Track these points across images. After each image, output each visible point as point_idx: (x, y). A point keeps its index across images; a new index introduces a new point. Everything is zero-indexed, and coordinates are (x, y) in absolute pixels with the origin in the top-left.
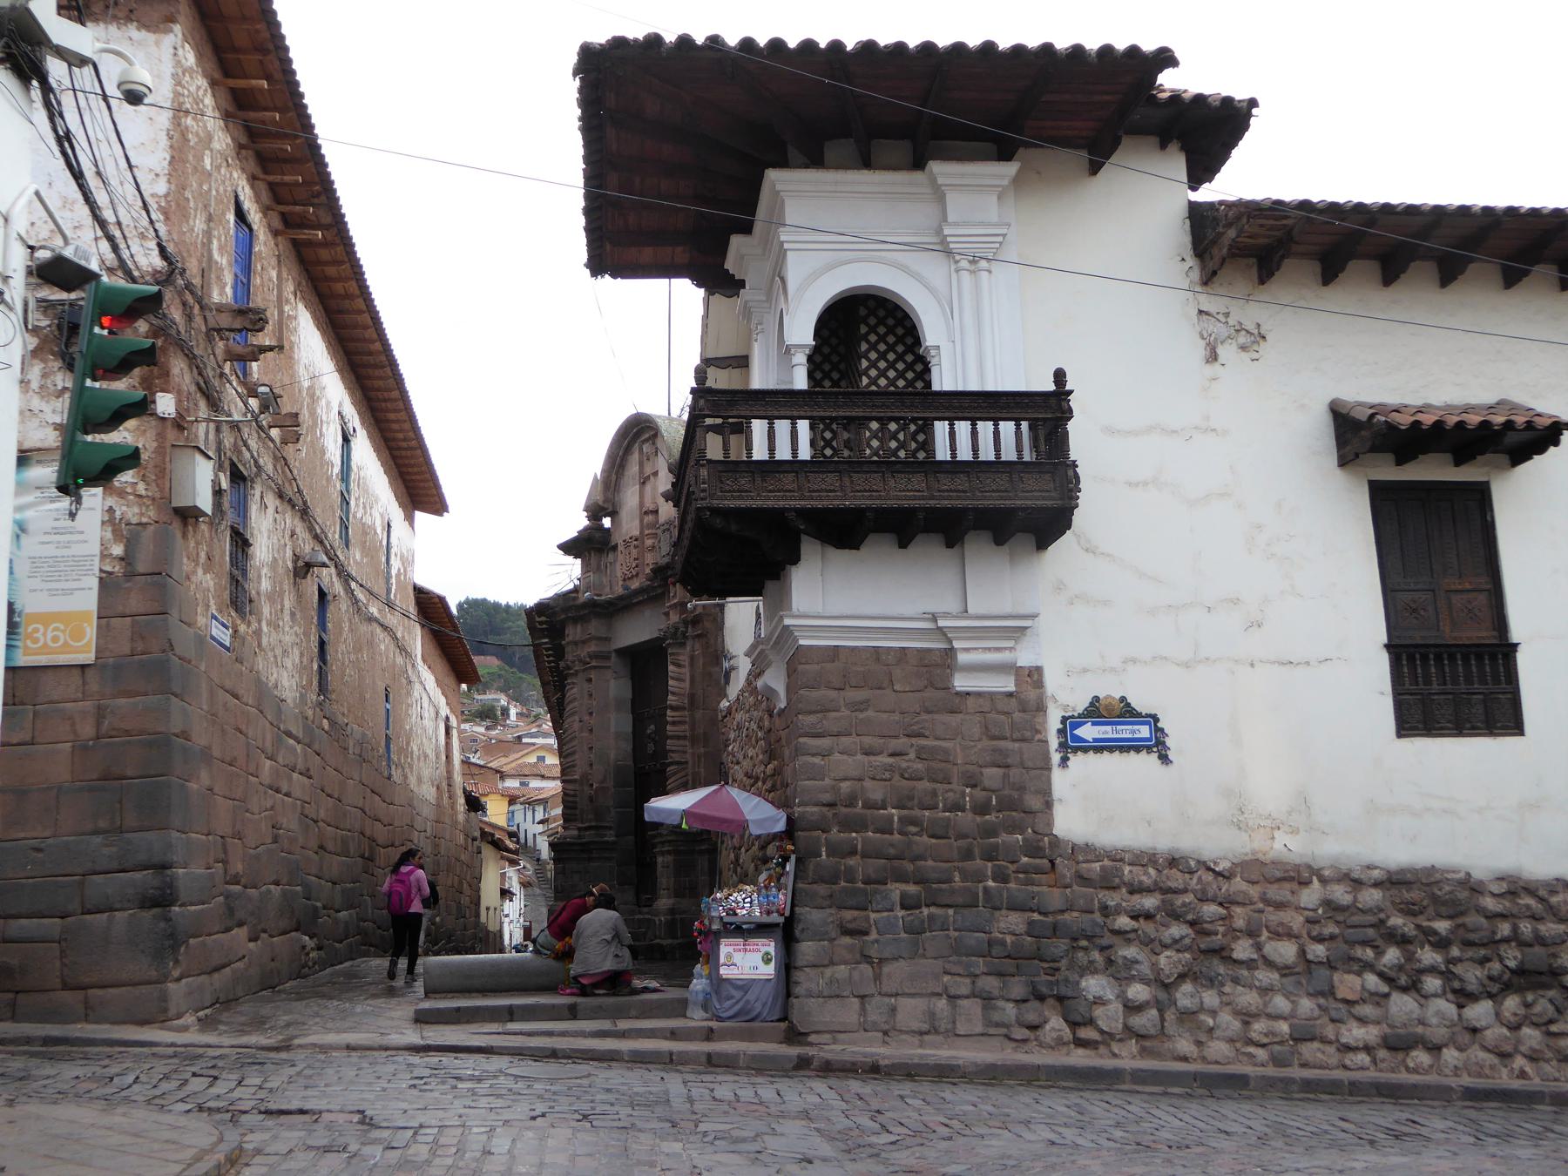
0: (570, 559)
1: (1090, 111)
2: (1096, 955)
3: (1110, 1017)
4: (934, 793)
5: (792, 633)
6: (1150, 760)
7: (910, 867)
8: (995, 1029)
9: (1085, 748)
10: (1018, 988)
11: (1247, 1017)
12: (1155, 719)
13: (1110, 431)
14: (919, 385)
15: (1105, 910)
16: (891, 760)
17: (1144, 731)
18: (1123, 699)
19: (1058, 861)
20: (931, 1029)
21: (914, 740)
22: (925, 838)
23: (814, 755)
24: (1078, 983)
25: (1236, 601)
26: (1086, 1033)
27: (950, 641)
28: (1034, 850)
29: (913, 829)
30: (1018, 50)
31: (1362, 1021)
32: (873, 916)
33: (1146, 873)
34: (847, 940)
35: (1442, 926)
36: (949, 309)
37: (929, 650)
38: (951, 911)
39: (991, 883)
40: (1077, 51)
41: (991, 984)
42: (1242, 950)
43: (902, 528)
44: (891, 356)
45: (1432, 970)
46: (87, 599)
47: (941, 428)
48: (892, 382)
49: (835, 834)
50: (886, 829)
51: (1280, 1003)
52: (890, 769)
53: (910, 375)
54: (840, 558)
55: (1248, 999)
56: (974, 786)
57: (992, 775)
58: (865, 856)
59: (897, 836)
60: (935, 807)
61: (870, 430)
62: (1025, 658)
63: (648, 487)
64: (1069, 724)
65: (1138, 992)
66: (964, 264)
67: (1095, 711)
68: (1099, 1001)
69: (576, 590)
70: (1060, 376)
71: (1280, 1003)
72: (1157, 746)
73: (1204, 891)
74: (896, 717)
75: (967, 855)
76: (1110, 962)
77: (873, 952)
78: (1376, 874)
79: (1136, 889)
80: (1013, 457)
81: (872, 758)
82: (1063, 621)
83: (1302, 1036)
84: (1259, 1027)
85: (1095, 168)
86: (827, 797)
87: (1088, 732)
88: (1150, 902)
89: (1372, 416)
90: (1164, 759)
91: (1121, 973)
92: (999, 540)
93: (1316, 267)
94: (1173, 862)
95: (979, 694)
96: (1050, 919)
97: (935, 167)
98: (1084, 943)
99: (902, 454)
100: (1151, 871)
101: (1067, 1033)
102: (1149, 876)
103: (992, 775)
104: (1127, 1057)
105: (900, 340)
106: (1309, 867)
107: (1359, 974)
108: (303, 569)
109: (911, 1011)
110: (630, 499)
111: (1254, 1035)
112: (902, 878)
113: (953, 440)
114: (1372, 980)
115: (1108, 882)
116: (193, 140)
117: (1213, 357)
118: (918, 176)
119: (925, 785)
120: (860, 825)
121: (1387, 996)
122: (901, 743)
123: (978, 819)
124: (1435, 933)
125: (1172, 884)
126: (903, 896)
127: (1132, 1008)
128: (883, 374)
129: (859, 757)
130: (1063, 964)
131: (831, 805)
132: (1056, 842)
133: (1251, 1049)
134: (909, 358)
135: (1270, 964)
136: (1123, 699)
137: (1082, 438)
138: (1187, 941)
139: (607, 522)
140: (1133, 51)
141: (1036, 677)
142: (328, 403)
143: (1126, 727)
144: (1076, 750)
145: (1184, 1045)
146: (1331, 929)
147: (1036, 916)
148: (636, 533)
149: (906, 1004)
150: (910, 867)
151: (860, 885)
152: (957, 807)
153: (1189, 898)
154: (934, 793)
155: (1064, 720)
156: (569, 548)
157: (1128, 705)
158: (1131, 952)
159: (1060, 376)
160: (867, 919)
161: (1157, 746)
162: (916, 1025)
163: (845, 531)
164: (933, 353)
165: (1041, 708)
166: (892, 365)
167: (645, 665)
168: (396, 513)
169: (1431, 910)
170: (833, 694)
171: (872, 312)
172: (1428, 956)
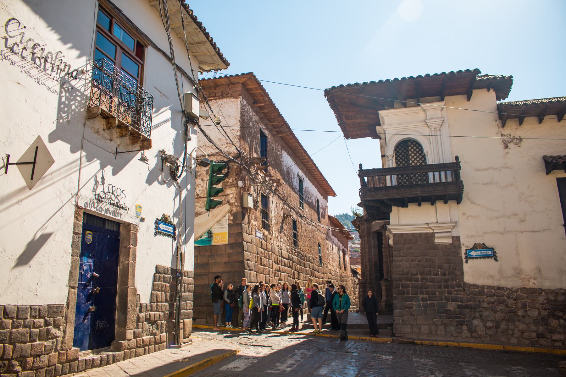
0: (360, 208)
4: (430, 271)
12: (493, 249)
13: (477, 170)
14: (423, 164)
16: (275, 229)
17: (490, 253)
18: (483, 244)
25: (516, 215)
26: (474, 335)
28: (459, 286)
39: (446, 295)
43: (419, 201)
44: (418, 155)
46: (226, 230)
47: (430, 175)
50: (417, 280)
52: (418, 265)
53: (421, 161)
54: (402, 210)
57: (446, 266)
60: (430, 274)
62: (455, 234)
65: (489, 324)
70: (457, 158)
72: (494, 256)
76: (481, 316)
78: (563, 291)
80: (438, 181)
86: (401, 273)
87: (473, 253)
90: (496, 260)
93: (537, 119)
94: (499, 288)
97: (423, 105)
99: (414, 183)
101: (469, 335)
106: (541, 289)
107: (558, 319)
108: (286, 216)
111: (525, 336)
112: (422, 293)
113: (432, 177)
116: (246, 121)
117: (506, 147)
118: (419, 108)
119: (428, 269)
120: (411, 280)
126: (422, 298)
127: (487, 328)
132: (465, 284)
137: (465, 174)
138: (504, 310)
142: (294, 174)
144: (470, 258)
147: (460, 303)
154: (430, 271)
155: (466, 250)
159: (457, 158)
160: (413, 304)
161: (494, 256)
165: (460, 247)
166: (418, 157)
168: (321, 198)
171: (412, 143)
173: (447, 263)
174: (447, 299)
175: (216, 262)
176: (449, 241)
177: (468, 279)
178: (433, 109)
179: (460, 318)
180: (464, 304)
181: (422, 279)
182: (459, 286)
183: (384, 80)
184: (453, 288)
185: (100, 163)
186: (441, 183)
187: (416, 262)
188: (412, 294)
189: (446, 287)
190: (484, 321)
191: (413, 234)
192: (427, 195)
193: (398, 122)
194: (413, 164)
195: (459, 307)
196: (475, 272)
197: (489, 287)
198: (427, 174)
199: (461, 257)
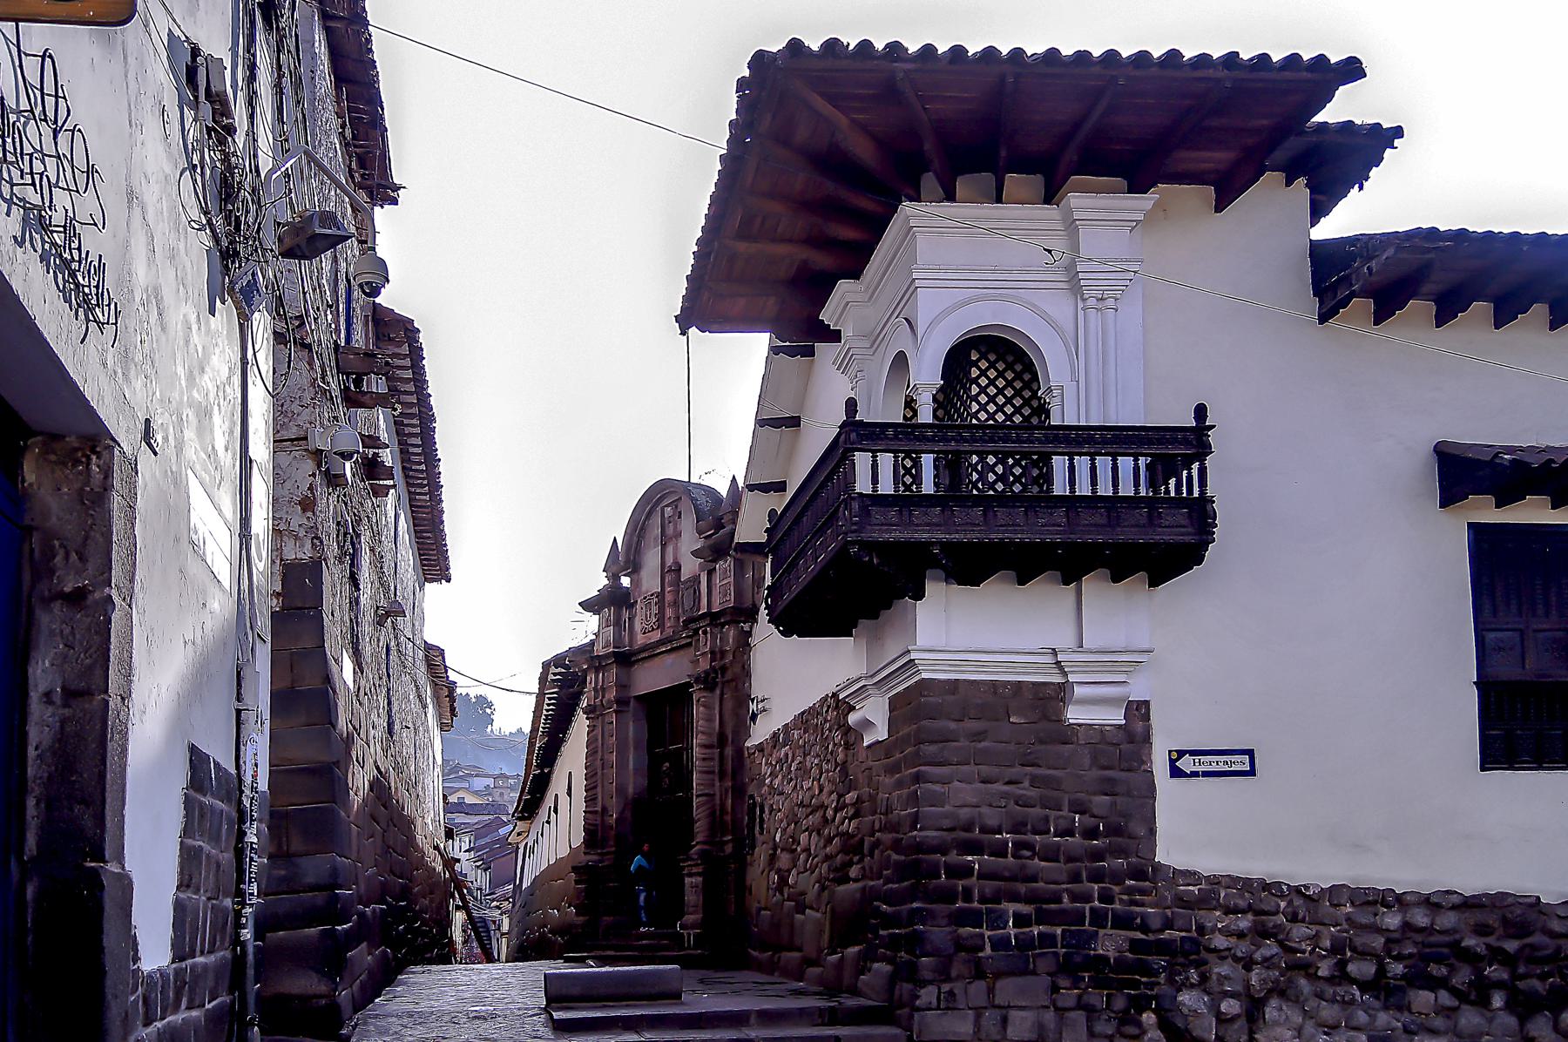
1: (1256, 127)
16: (1006, 788)
27: (1065, 674)
29: (1028, 853)
35: (1511, 946)
43: (1025, 564)
45: (1499, 985)
47: (1059, 463)
48: (1009, 417)
49: (953, 857)
50: (1000, 851)
52: (1004, 796)
57: (1100, 802)
58: (981, 876)
65: (1230, 1006)
66: (1092, 302)
69: (592, 643)
70: (1201, 411)
74: (1012, 747)
75: (1075, 878)
76: (1204, 978)
78: (1455, 899)
86: (946, 823)
88: (1244, 922)
89: (1496, 455)
94: (1265, 886)
103: (1100, 802)
105: (1018, 376)
110: (652, 560)
112: (1014, 897)
113: (1070, 476)
114: (1445, 998)
115: (1205, 901)
118: (1050, 211)
120: (975, 848)
121: (1455, 1009)
122: (1017, 771)
123: (1087, 842)
124: (1504, 950)
125: (1266, 908)
128: (1000, 409)
132: (1158, 867)
134: (1027, 394)
137: (1225, 478)
139: (625, 581)
140: (1321, 60)
151: (976, 904)
154: (1047, 819)
156: (587, 605)
158: (1223, 969)
159: (1201, 411)
160: (982, 936)
163: (970, 567)
165: (1147, 739)
167: (665, 711)
169: (1500, 931)
170: (953, 725)
172: (1493, 971)
174: (1098, 918)
176: (1117, 717)
177: (1168, 853)
178: (1103, 217)
179: (1135, 985)
180: (1151, 937)
181: (1018, 846)
182: (1139, 874)
183: (1096, 53)
184: (1120, 882)
185: (136, 959)
186: (1094, 501)
188: (983, 900)
189: (1096, 877)
190: (1217, 997)
194: (983, 416)
196: (1192, 833)
197: (1233, 881)
198: (1046, 459)
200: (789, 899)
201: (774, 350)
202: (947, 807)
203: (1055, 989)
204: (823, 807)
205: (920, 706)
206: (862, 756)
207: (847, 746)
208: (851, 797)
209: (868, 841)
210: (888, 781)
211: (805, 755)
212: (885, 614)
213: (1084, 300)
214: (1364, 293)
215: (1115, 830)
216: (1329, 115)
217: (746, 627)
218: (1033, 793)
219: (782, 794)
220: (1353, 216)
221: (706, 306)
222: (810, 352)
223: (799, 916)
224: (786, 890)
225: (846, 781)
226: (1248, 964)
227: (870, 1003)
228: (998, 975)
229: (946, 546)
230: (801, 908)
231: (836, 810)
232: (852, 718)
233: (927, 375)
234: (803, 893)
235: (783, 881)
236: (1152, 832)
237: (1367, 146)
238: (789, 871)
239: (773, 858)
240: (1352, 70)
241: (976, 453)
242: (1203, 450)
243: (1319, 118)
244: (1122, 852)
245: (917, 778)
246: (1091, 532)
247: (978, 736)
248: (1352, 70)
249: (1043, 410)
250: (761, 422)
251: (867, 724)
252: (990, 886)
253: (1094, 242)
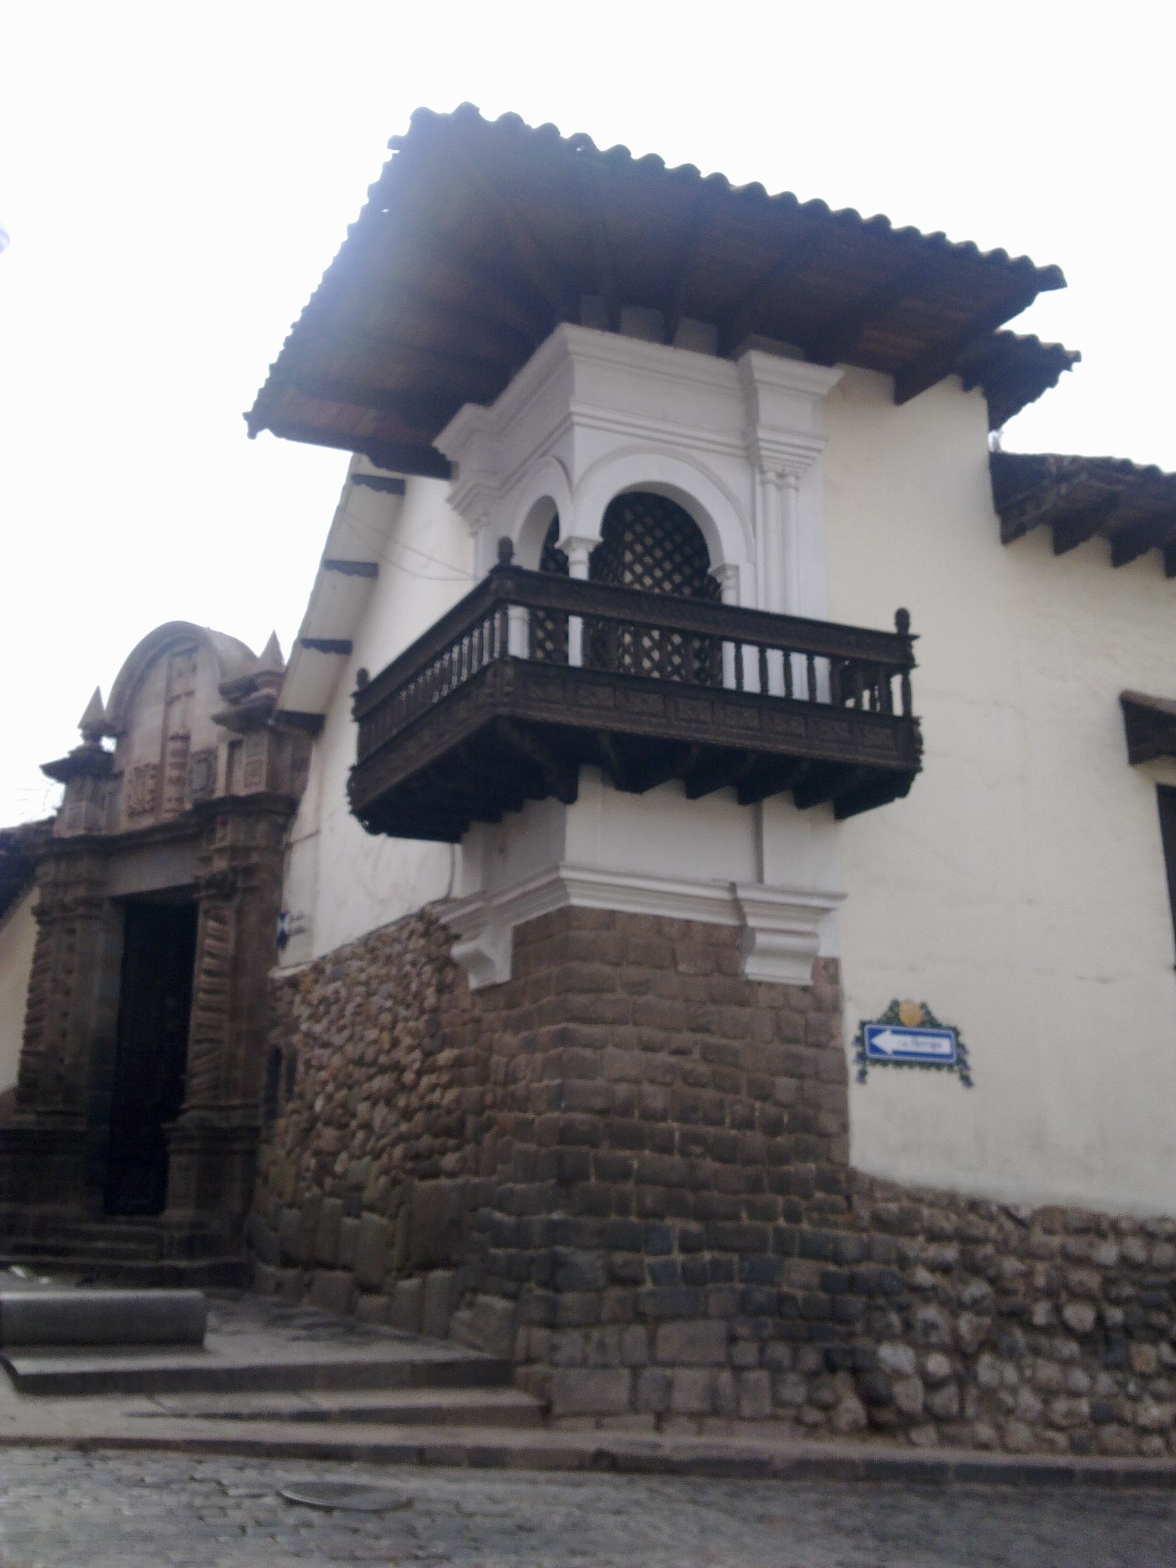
2: (894, 1318)
3: (909, 1395)
4: (720, 1105)
5: (564, 887)
6: (950, 1080)
7: (690, 1197)
8: (780, 1413)
9: (883, 1061)
10: (811, 1359)
11: (1047, 1394)
15: (904, 1262)
16: (673, 1059)
17: (945, 1046)
19: (855, 1198)
20: (715, 1410)
21: (700, 1037)
22: (709, 1161)
23: (585, 1046)
24: (875, 1352)
27: (742, 916)
30: (910, 233)
31: (1158, 1398)
32: (648, 1260)
33: (947, 1218)
34: (617, 1292)
36: (750, 521)
37: (716, 927)
38: (736, 1258)
40: (969, 248)
41: (780, 1351)
42: (1041, 1313)
49: (605, 1151)
51: (1080, 1379)
55: (1048, 1372)
56: (765, 1098)
57: (785, 1086)
59: (677, 1158)
61: (672, 644)
62: (825, 951)
63: (177, 709)
64: (869, 1031)
65: (938, 1364)
66: (771, 476)
67: (893, 1018)
68: (898, 1375)
69: (51, 821)
70: (902, 617)
71: (1080, 1379)
72: (957, 1063)
73: (1006, 1242)
75: (755, 1186)
76: (908, 1325)
77: (649, 1308)
79: (935, 1236)
81: (650, 1055)
82: (864, 908)
83: (1102, 1416)
84: (1061, 1406)
85: (902, 394)
86: (599, 1102)
87: (888, 1042)
88: (950, 1253)
90: (966, 1081)
91: (917, 1338)
92: (803, 801)
94: (974, 1205)
95: (771, 986)
96: (845, 1271)
98: (881, 1301)
100: (953, 1217)
102: (948, 1222)
104: (925, 1448)
109: (689, 1387)
112: (682, 1212)
115: (901, 1225)
120: (634, 1140)
122: (684, 1038)
127: (932, 1384)
129: (637, 1052)
130: (859, 1326)
131: (603, 1112)
132: (853, 1176)
133: (1051, 1434)
135: (1069, 1331)
136: (923, 1006)
137: (934, 693)
139: (108, 744)
140: (1024, 262)
141: (831, 970)
143: (934, 1044)
145: (985, 1431)
146: (1128, 1291)
147: (832, 1268)
148: (155, 759)
149: (684, 1376)
150: (690, 1197)
151: (633, 1219)
152: (747, 1124)
153: (989, 1249)
155: (863, 1025)
156: (53, 770)
157: (928, 1013)
158: (930, 1313)
159: (902, 617)
161: (957, 1063)
162: (695, 1405)
164: (729, 573)
170: (607, 970)
173: (791, 1075)
175: (614, 1247)
187: (664, 1057)
189: (782, 1186)
191: (658, 919)
192: (783, 748)
193: (618, 422)
195: (827, 1283)
199: (840, 1051)
200: (332, 1194)
201: (356, 478)
202: (600, 1082)
203: (732, 1339)
204: (398, 1068)
205: (549, 939)
206: (465, 1003)
207: (441, 989)
208: (445, 1056)
209: (471, 1121)
210: (510, 1039)
211: (369, 995)
212: (511, 818)
213: (763, 472)
214: (1042, 519)
215: (804, 1124)
216: (1018, 325)
217: (280, 820)
218: (704, 1069)
219: (324, 1052)
220: (1032, 431)
221: (291, 405)
222: (398, 488)
223: (350, 1222)
224: (329, 1182)
225: (436, 1036)
226: (955, 1307)
227: (473, 1354)
228: (659, 1319)
229: (618, 738)
230: (355, 1209)
231: (419, 1074)
232: (458, 951)
233: (583, 525)
234: (359, 1188)
235: (325, 1169)
236: (845, 1128)
237: (1041, 366)
238: (335, 1154)
239: (308, 1131)
240: (1052, 279)
241: (659, 628)
242: (906, 664)
243: (1005, 327)
244: (806, 1154)
245: (563, 1038)
246: (781, 741)
247: (640, 987)
248: (1052, 279)
249: (713, 588)
250: (330, 564)
251: (479, 960)
252: (652, 1196)
253: (770, 409)
